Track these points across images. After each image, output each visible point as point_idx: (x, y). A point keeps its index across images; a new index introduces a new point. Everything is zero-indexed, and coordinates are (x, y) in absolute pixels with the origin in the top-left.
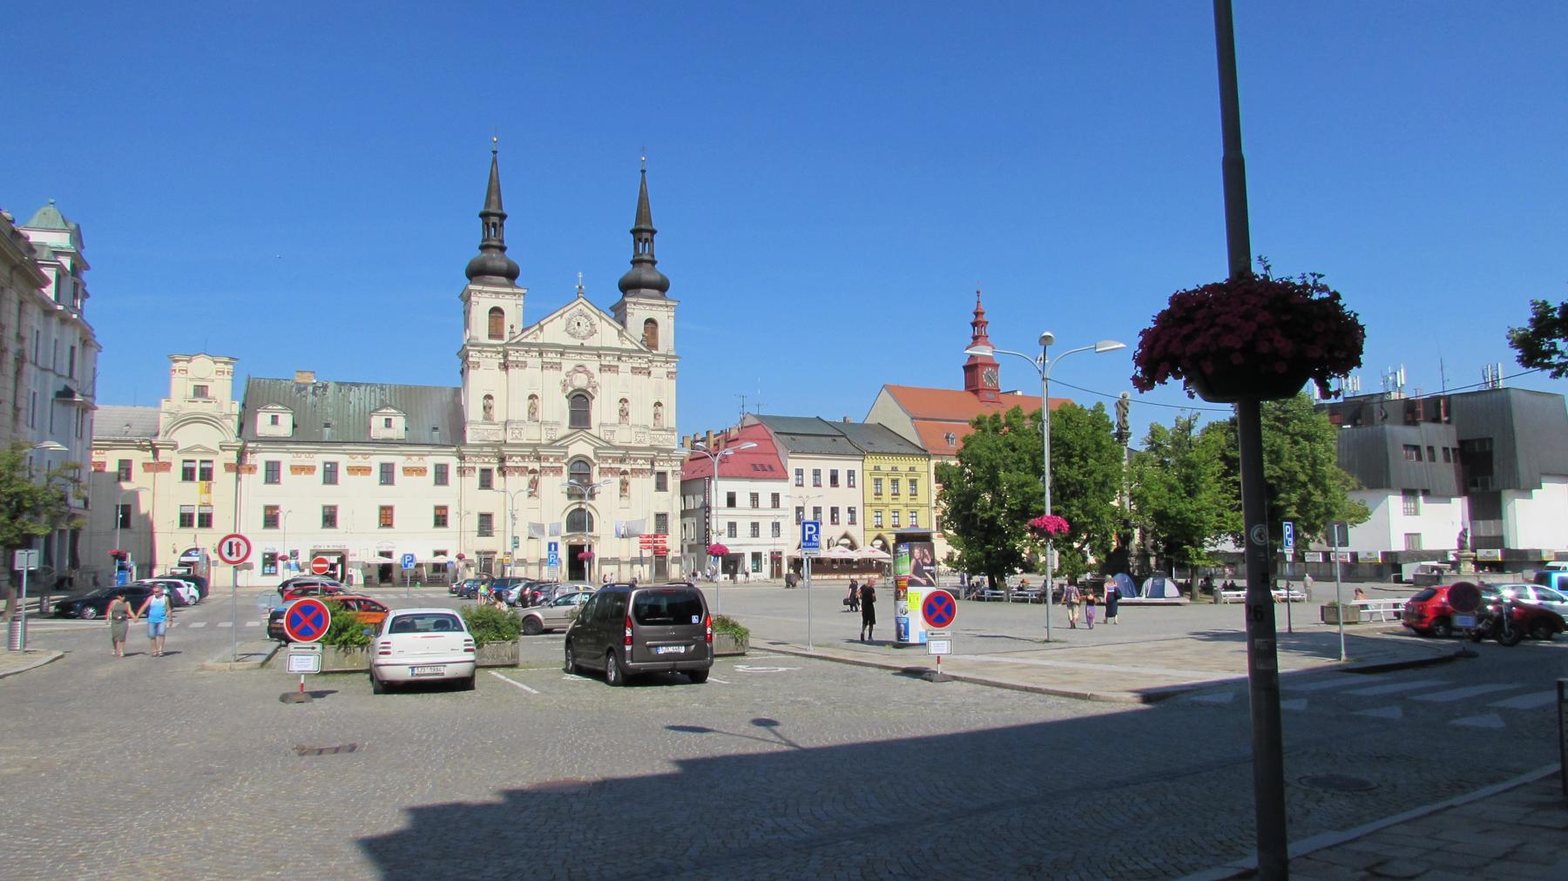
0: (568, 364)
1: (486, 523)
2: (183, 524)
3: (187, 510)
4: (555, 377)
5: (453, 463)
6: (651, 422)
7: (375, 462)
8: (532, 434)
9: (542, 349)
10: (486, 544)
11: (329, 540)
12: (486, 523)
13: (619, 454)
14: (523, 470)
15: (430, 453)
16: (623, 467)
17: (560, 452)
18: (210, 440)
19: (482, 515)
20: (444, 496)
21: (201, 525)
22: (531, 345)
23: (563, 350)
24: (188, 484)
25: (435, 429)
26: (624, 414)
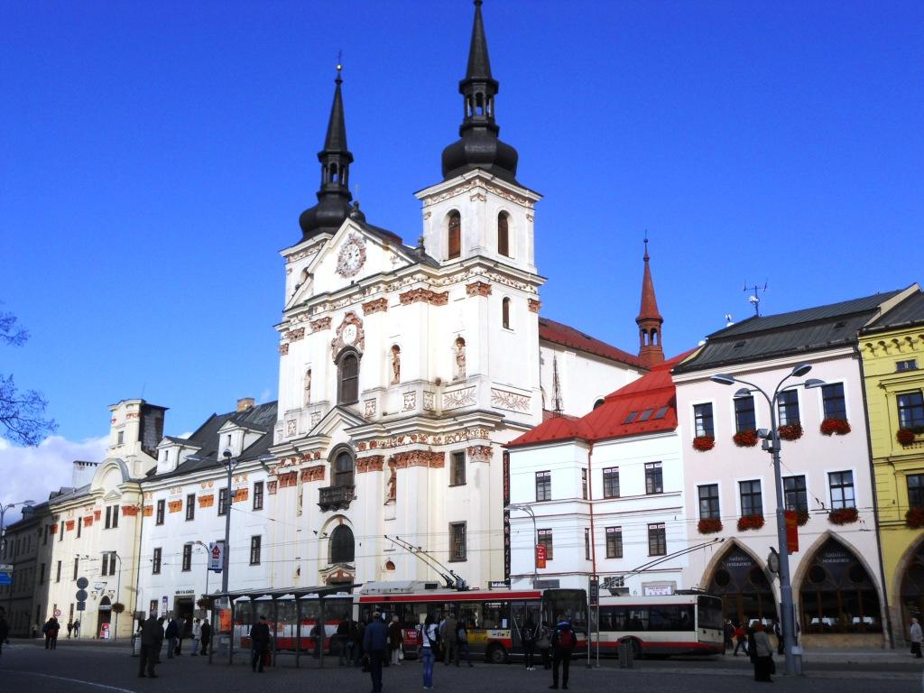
4: (328, 335)
14: (376, 462)
23: (328, 298)
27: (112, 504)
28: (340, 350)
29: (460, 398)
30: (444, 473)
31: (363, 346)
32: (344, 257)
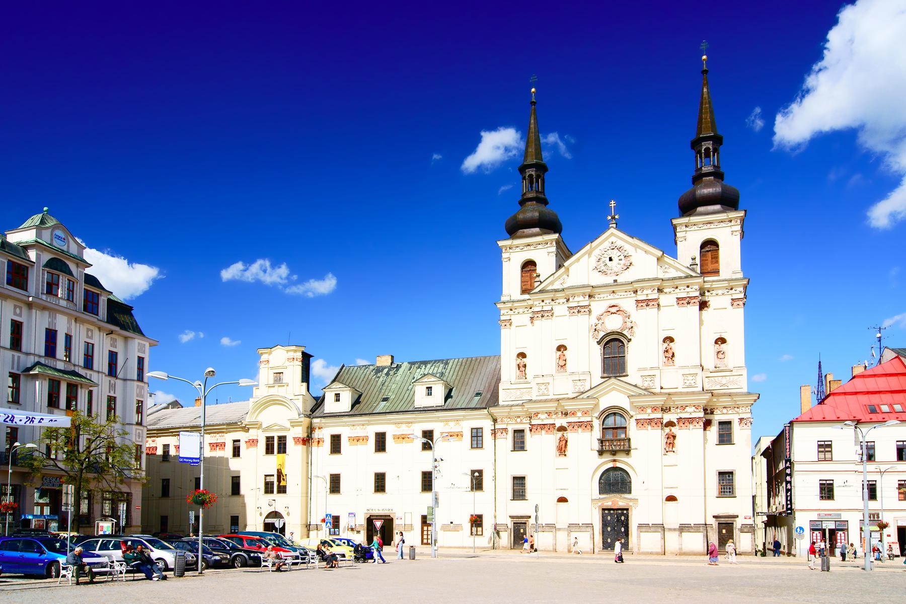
0: (598, 306)
1: (519, 486)
2: (266, 492)
3: (269, 479)
4: (583, 322)
5: (487, 425)
6: (710, 362)
7: (417, 429)
8: (563, 386)
9: (567, 293)
10: (520, 508)
11: (380, 504)
12: (519, 486)
13: (659, 401)
15: (465, 418)
16: (667, 417)
17: (588, 405)
18: (286, 418)
19: (515, 478)
20: (480, 459)
21: (279, 492)
22: (556, 291)
24: (270, 457)
25: (478, 394)
26: (670, 356)
27: (276, 435)
28: (602, 334)
29: (724, 381)
30: (714, 430)
32: (603, 259)
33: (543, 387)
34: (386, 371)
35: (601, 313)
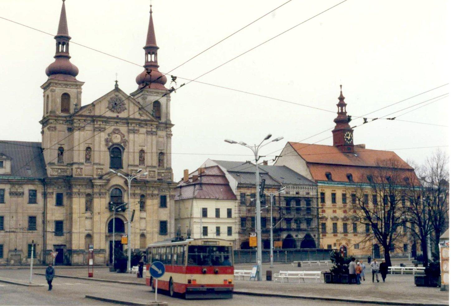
0: (110, 129)
20: (35, 209)
26: (142, 160)
28: (111, 144)
31: (125, 145)
33: (79, 170)
34: (396, 225)
35: (110, 132)
